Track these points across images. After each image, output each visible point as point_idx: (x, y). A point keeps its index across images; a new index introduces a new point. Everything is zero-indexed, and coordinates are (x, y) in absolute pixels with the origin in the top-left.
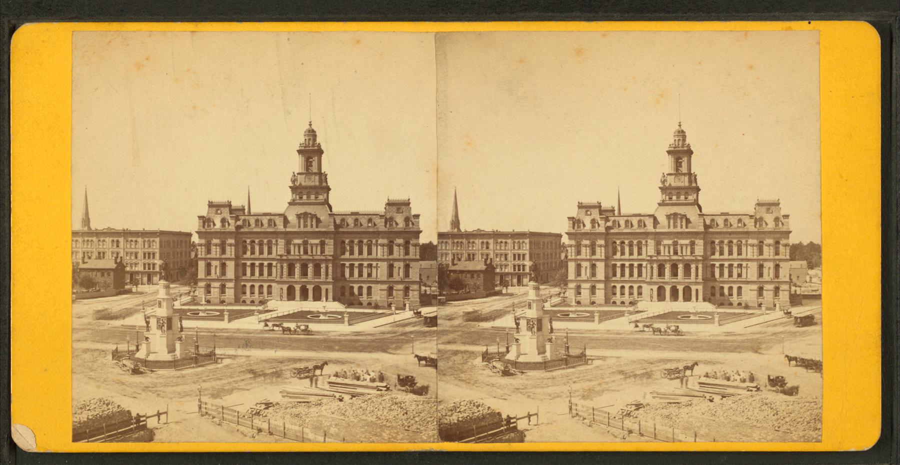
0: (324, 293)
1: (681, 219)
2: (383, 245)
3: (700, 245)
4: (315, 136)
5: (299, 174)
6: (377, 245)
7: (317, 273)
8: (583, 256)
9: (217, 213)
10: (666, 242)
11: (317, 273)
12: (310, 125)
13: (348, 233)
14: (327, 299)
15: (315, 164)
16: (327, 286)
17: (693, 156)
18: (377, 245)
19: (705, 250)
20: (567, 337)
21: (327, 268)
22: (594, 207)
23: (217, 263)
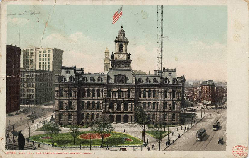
0: (130, 118)
1: (122, 78)
2: (161, 93)
3: (133, 91)
4: (124, 34)
5: (116, 53)
6: (158, 92)
7: (126, 108)
8: (168, 98)
9: (67, 73)
10: (114, 90)
11: (126, 108)
12: (122, 28)
13: (142, 85)
14: (131, 121)
15: (124, 49)
16: (132, 115)
17: (128, 44)
18: (158, 92)
19: (136, 95)
20: (91, 147)
21: (132, 105)
22: (72, 69)
23: (171, 102)
